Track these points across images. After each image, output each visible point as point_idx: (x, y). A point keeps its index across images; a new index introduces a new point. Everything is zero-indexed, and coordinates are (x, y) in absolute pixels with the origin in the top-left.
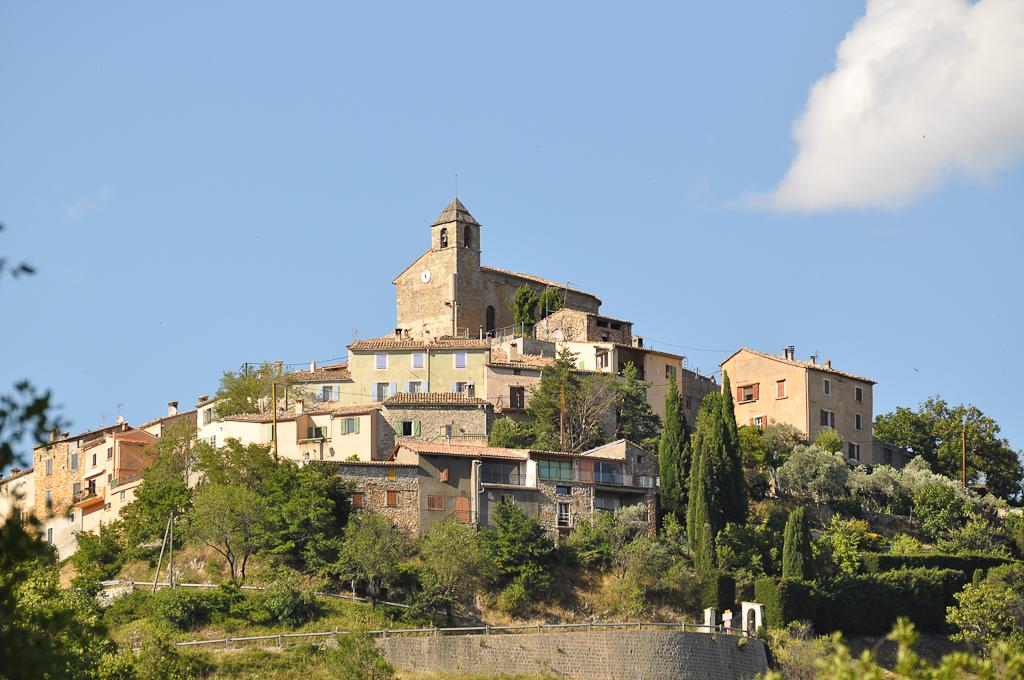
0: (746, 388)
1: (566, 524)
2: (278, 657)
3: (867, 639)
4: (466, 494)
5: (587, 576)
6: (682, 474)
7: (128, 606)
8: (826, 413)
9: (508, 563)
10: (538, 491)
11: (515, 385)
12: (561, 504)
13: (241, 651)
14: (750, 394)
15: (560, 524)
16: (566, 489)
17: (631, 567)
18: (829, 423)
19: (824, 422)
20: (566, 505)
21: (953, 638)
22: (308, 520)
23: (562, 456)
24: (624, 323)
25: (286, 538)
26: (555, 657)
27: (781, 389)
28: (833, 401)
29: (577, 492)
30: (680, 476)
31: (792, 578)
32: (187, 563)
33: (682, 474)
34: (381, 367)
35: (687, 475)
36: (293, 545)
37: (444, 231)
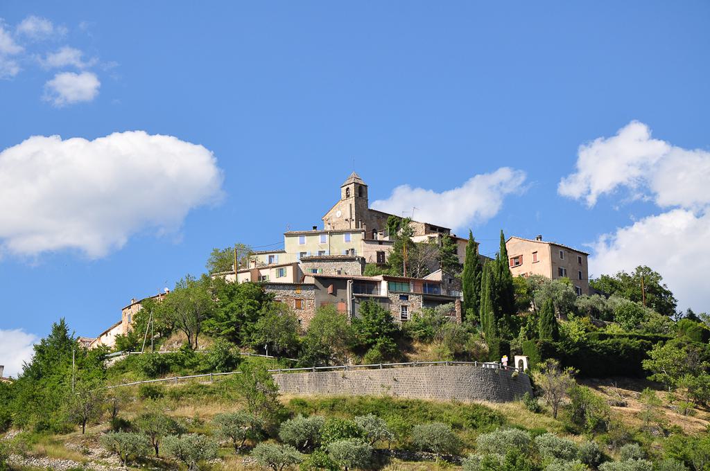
0: (515, 258)
1: (406, 318)
2: (208, 387)
3: (594, 380)
4: (343, 301)
5: (416, 345)
6: (477, 288)
7: (121, 365)
8: (562, 270)
9: (368, 337)
10: (388, 298)
11: (379, 250)
12: (402, 306)
13: (184, 384)
14: (518, 261)
15: (402, 318)
16: (404, 297)
17: (445, 339)
18: (564, 273)
19: (561, 274)
20: (406, 307)
21: (649, 378)
22: (242, 313)
23: (403, 279)
24: (446, 229)
25: (229, 326)
26: (392, 383)
27: (535, 257)
28: (565, 262)
29: (412, 298)
30: (475, 291)
31: (546, 340)
32: (170, 344)
33: (477, 288)
34: (302, 243)
35: (480, 290)
36: (234, 329)
37: (348, 189)
